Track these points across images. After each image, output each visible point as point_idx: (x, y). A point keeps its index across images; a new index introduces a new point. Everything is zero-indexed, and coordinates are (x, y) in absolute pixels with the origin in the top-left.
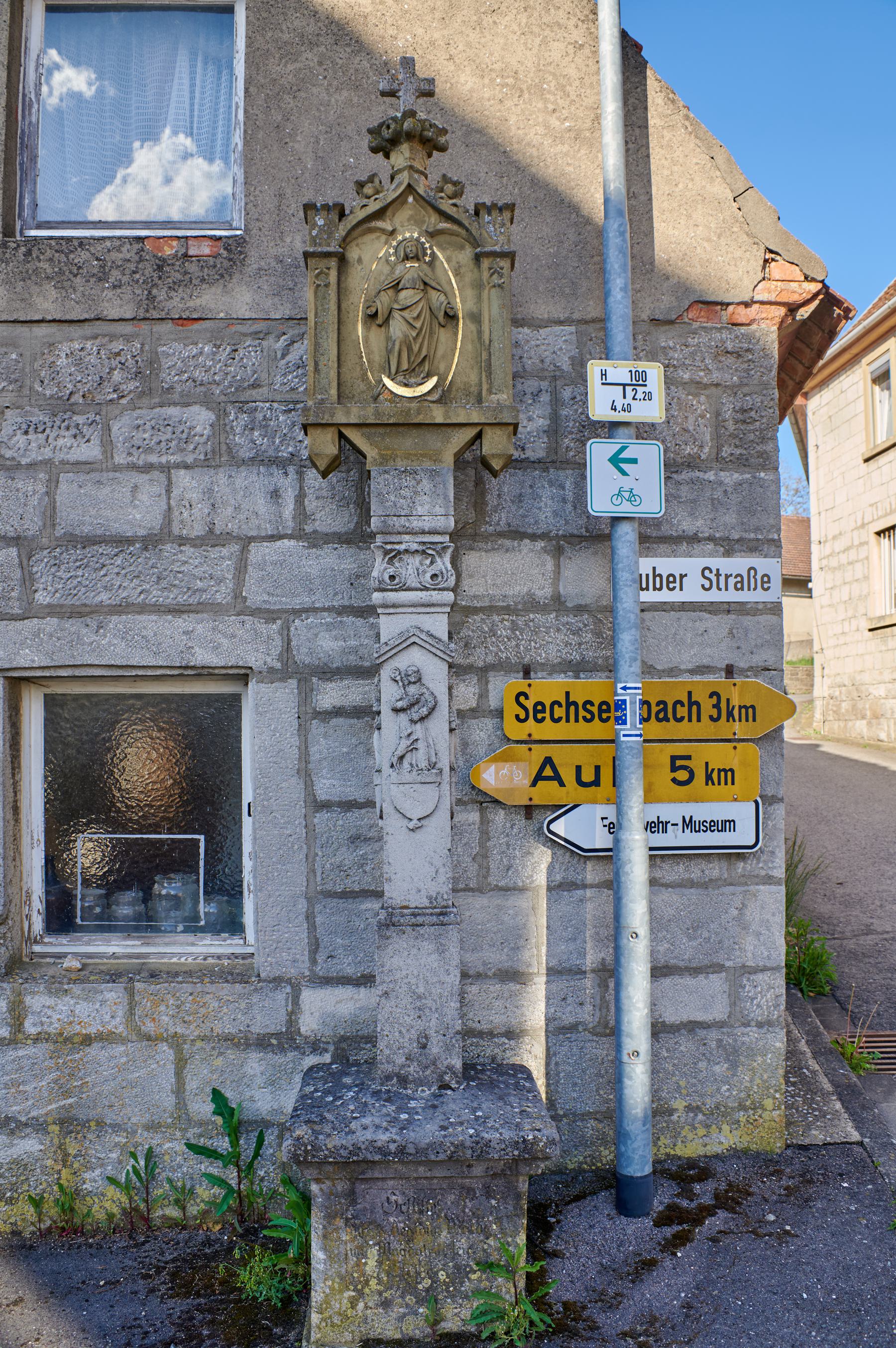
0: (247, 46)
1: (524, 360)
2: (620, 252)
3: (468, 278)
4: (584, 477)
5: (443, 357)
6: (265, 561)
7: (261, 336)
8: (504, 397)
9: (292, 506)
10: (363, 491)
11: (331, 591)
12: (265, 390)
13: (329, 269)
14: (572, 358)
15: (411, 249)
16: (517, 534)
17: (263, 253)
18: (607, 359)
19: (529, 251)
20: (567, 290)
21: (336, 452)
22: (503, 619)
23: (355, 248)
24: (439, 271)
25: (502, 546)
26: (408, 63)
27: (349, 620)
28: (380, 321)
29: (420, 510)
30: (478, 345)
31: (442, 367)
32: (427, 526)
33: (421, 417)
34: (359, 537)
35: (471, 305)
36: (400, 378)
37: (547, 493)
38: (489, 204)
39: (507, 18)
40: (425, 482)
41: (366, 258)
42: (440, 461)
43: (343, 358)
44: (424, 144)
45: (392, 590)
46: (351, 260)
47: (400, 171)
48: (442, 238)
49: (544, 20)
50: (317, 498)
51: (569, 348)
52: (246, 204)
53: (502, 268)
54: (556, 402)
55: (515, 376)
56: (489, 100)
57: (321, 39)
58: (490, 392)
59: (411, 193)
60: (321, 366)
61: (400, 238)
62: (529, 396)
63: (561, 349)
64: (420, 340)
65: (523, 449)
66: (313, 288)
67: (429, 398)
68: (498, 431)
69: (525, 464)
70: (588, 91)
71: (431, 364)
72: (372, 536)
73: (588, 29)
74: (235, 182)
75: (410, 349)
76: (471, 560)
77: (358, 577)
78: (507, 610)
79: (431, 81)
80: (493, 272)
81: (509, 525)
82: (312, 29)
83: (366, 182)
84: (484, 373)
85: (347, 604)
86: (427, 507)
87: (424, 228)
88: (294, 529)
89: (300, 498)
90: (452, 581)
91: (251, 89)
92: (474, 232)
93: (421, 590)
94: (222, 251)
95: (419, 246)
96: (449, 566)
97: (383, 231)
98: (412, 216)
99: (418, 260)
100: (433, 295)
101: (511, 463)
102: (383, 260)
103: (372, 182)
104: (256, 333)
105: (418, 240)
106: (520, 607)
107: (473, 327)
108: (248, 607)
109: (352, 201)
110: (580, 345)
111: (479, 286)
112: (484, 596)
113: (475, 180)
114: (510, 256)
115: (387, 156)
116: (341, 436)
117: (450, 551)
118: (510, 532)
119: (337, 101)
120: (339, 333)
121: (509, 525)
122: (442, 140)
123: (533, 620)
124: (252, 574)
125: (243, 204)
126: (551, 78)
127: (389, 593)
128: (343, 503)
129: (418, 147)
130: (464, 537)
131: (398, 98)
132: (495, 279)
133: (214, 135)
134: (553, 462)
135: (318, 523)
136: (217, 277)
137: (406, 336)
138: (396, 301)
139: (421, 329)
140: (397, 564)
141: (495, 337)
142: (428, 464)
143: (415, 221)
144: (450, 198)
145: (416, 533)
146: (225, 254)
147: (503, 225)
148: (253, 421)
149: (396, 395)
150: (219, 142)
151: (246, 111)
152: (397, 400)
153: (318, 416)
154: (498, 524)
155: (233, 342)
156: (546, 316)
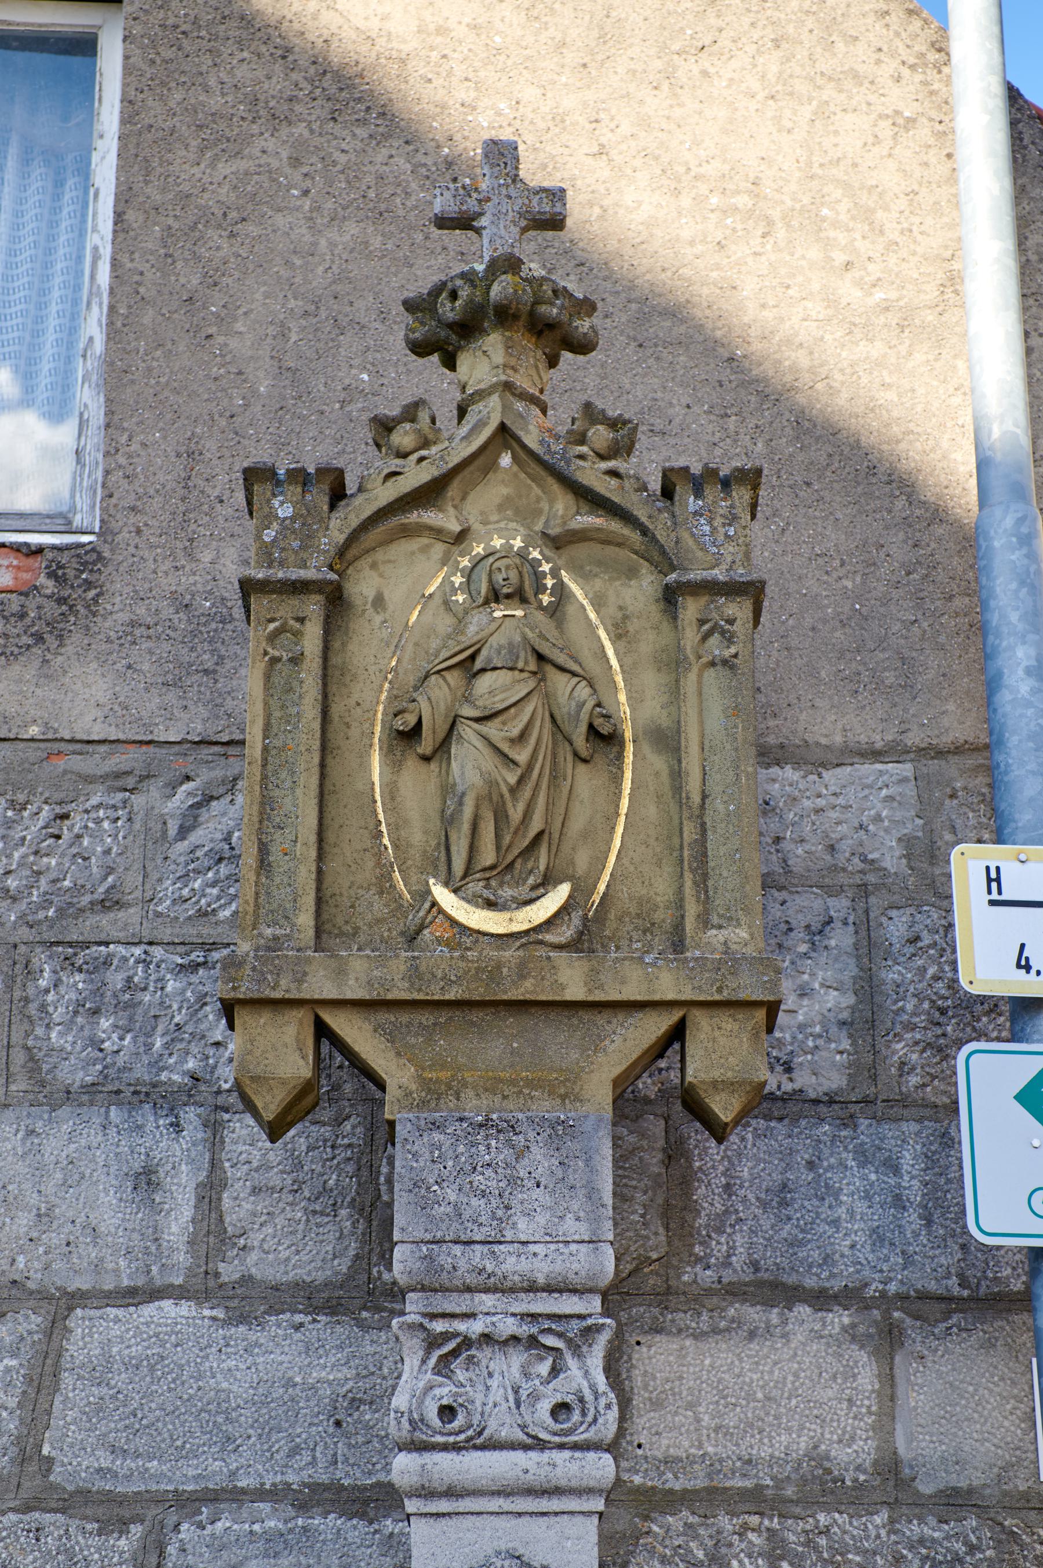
0: (123, 122)
1: (786, 845)
2: (1022, 583)
3: (649, 643)
4: (949, 1141)
5: (586, 835)
6: (109, 1359)
7: (130, 782)
8: (739, 935)
9: (187, 1213)
10: (374, 1171)
11: (281, 1443)
12: (132, 915)
13: (301, 620)
14: (906, 841)
15: (506, 577)
16: (778, 1292)
17: (142, 587)
18: (999, 840)
19: (793, 586)
20: (890, 677)
21: (306, 1071)
22: (746, 1527)
23: (367, 572)
24: (574, 629)
25: (737, 1322)
26: (502, 154)
27: (326, 1523)
28: (426, 745)
29: (524, 1228)
30: (674, 808)
31: (582, 861)
32: (541, 1271)
33: (528, 984)
34: (361, 1296)
35: (654, 709)
36: (475, 887)
37: (853, 1182)
38: (696, 469)
39: (734, 64)
40: (537, 1152)
41: (394, 596)
42: (578, 1099)
43: (330, 837)
44: (539, 334)
45: (445, 1448)
46: (358, 601)
47: (480, 395)
48: (581, 551)
49: (820, 66)
50: (255, 1191)
51: (898, 815)
52: (107, 472)
53: (731, 622)
54: (869, 949)
55: (768, 883)
56: (692, 243)
57: (298, 108)
58: (704, 922)
59: (507, 446)
60: (275, 855)
61: (479, 550)
62: (799, 934)
63: (878, 819)
64: (527, 793)
65: (788, 1069)
66: (261, 666)
67: (549, 938)
68: (727, 1022)
69: (793, 1107)
70: (929, 221)
71: (555, 852)
72: (397, 1293)
73: (925, 83)
74: (83, 424)
75: (501, 816)
76: (657, 1359)
77: (355, 1403)
78: (756, 1500)
79: (558, 195)
80: (709, 629)
81: (756, 1266)
82: (277, 85)
83: (398, 421)
84: (688, 877)
85: (325, 1478)
86: (541, 1219)
87: (539, 527)
88: (190, 1273)
89: (210, 1192)
90: (608, 1425)
91: (130, 216)
92: (661, 535)
93: (526, 1448)
94: (42, 580)
95: (527, 569)
96: (601, 1380)
97: (438, 533)
98: (508, 499)
99: (524, 600)
100: (561, 683)
101: (762, 1103)
102: (438, 600)
103: (413, 420)
104: (118, 775)
105: (522, 555)
106: (790, 1492)
107: (659, 763)
108: (54, 1487)
109: (360, 461)
110: (926, 808)
111: (674, 664)
112: (691, 1460)
113: (659, 424)
114: (753, 591)
115: (450, 363)
116: (322, 1031)
117: (603, 1339)
118: (760, 1284)
119: (332, 245)
120: (323, 776)
121: (756, 1266)
122: (583, 325)
123: (826, 1531)
124: (73, 1394)
125: (100, 474)
126: (838, 193)
127: (439, 1457)
128: (324, 1203)
129: (524, 341)
130: (642, 1295)
131: (478, 231)
132: (715, 646)
133: (39, 320)
134: (866, 1101)
135: (253, 1257)
136: (26, 640)
137: (492, 784)
138: (467, 699)
139: (530, 767)
140: (461, 1375)
141: (715, 787)
142: (545, 1107)
143: (517, 511)
144: (602, 457)
145: (512, 1290)
146: (49, 586)
147: (732, 519)
148: (98, 992)
149: (465, 929)
150: (51, 337)
151: (115, 264)
152: (468, 941)
153: (261, 980)
154: (727, 1264)
155: (58, 796)
156: (838, 739)
